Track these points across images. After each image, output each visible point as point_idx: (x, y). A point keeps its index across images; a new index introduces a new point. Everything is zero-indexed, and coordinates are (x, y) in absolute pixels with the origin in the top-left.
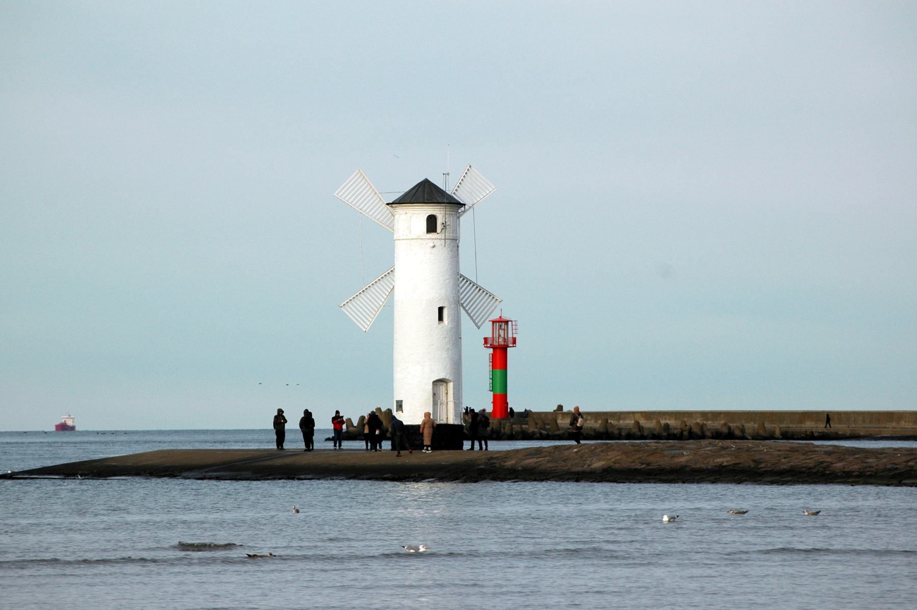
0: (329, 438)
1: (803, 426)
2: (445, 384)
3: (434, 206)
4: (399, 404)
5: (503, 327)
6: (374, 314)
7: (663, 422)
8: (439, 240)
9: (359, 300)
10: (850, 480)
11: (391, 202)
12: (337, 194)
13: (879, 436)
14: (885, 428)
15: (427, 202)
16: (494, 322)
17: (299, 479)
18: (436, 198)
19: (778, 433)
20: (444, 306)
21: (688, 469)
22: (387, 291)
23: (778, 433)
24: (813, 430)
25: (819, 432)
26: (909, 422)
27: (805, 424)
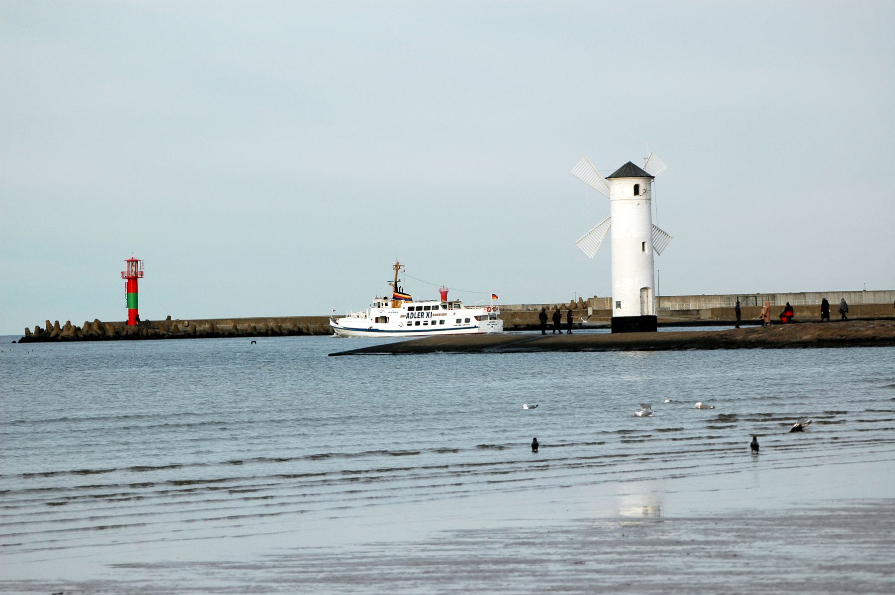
5: (134, 265)
7: (252, 325)
16: (128, 261)
17: (584, 351)
21: (878, 338)
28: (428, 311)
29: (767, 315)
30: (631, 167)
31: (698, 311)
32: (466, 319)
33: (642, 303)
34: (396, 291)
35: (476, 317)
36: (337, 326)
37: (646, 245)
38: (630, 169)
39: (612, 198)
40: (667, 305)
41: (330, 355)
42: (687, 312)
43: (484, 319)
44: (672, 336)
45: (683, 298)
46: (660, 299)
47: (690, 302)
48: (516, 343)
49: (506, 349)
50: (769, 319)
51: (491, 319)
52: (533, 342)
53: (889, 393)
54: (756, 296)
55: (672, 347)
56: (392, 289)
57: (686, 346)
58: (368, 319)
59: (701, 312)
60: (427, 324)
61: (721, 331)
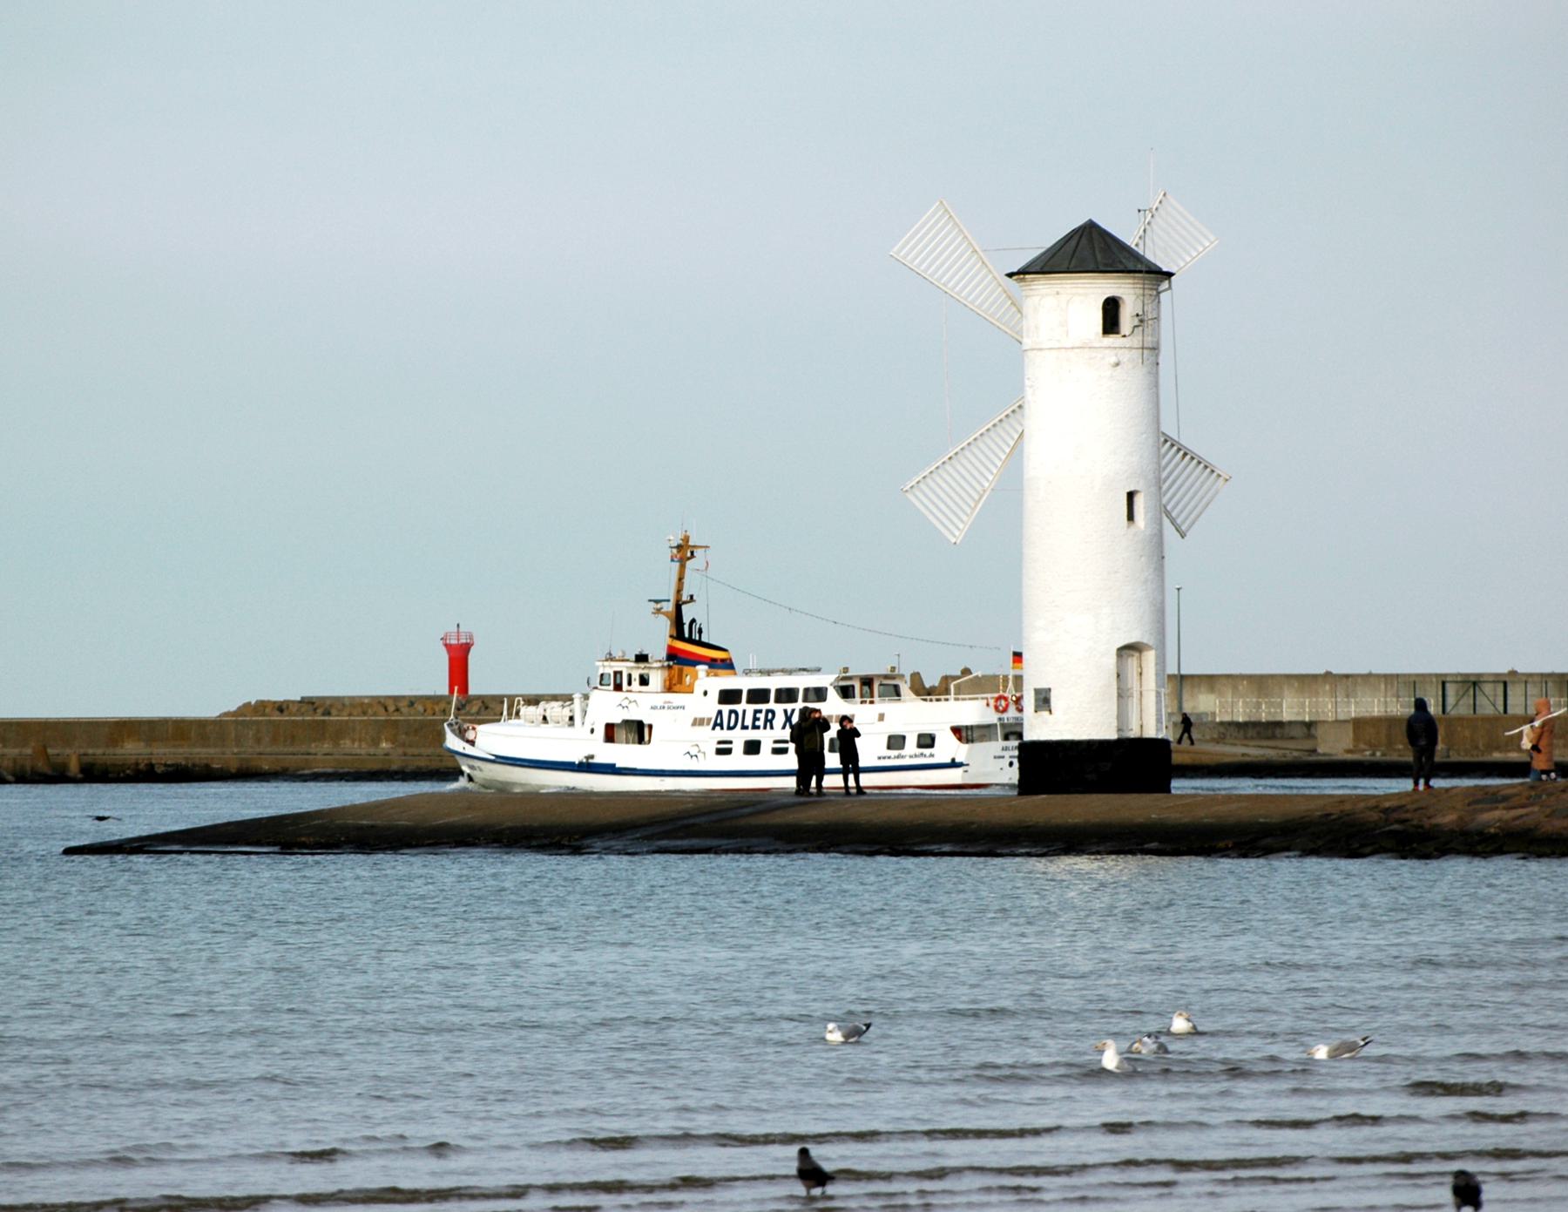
0: (573, 763)
1: (119, 751)
2: (1137, 654)
3: (1119, 278)
4: (1042, 697)
6: (973, 505)
8: (1126, 351)
9: (941, 477)
10: (1023, 851)
11: (1015, 270)
12: (898, 252)
13: (306, 772)
14: (309, 754)
15: (1102, 268)
18: (1121, 262)
19: (74, 768)
20: (1137, 489)
22: (1004, 451)
23: (74, 768)
24: (154, 762)
25: (166, 765)
26: (360, 740)
27: (122, 747)
28: (789, 707)
29: (1540, 747)
30: (1095, 235)
31: (1309, 725)
32: (920, 736)
33: (1122, 695)
34: (679, 635)
35: (957, 731)
36: (469, 750)
37: (1140, 503)
38: (1093, 248)
39: (1027, 342)
40: (1204, 704)
41: (69, 851)
42: (1272, 729)
43: (982, 739)
44: (1222, 810)
45: (1262, 684)
46: (1181, 682)
47: (1281, 696)
48: (697, 820)
49: (664, 843)
50: (1550, 760)
51: (1006, 738)
52: (754, 821)
53: (669, 990)
54: (1505, 682)
55: (1221, 845)
56: (664, 626)
57: (1268, 841)
58: (580, 730)
59: (1319, 732)
60: (728, 752)
61: (1387, 797)
